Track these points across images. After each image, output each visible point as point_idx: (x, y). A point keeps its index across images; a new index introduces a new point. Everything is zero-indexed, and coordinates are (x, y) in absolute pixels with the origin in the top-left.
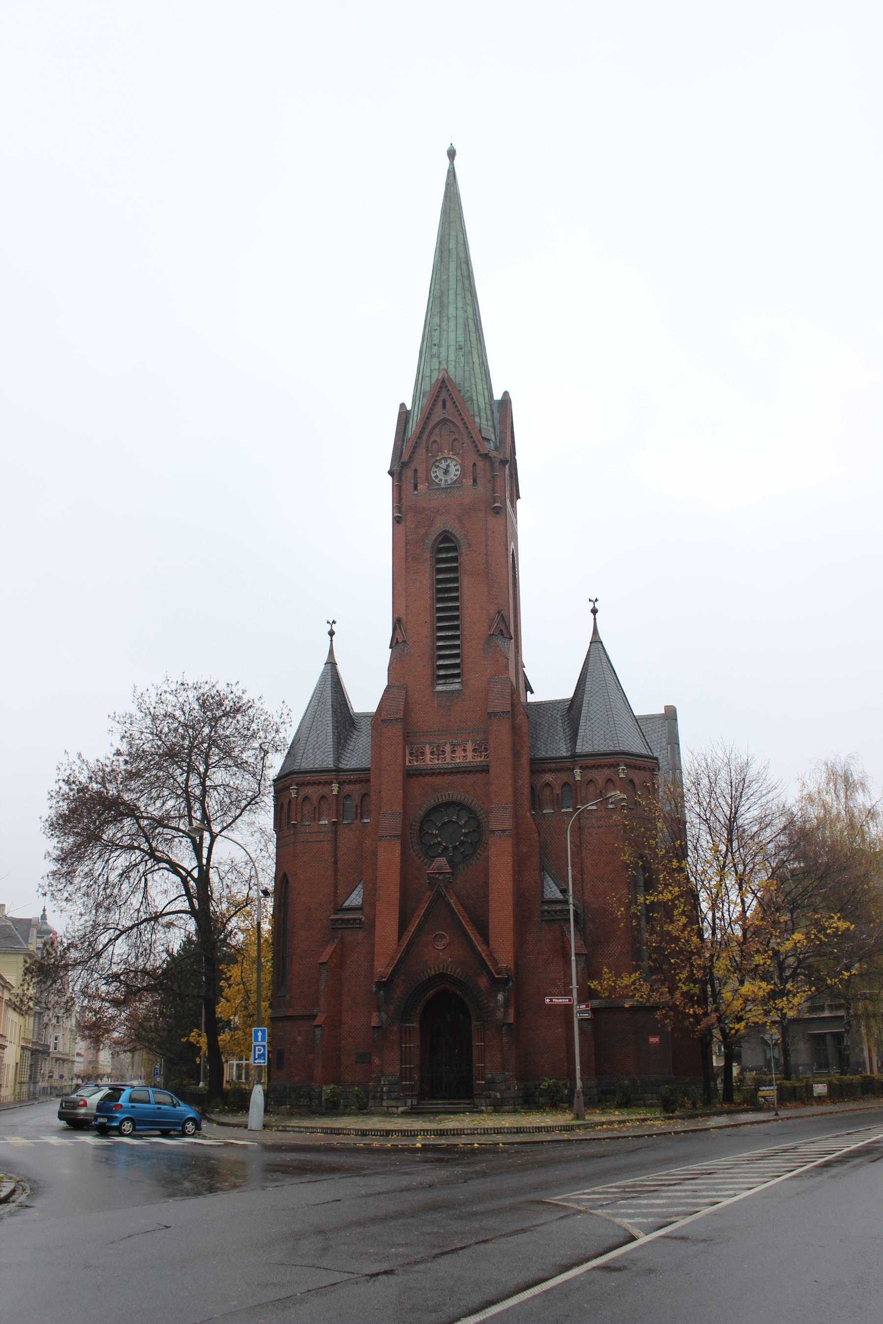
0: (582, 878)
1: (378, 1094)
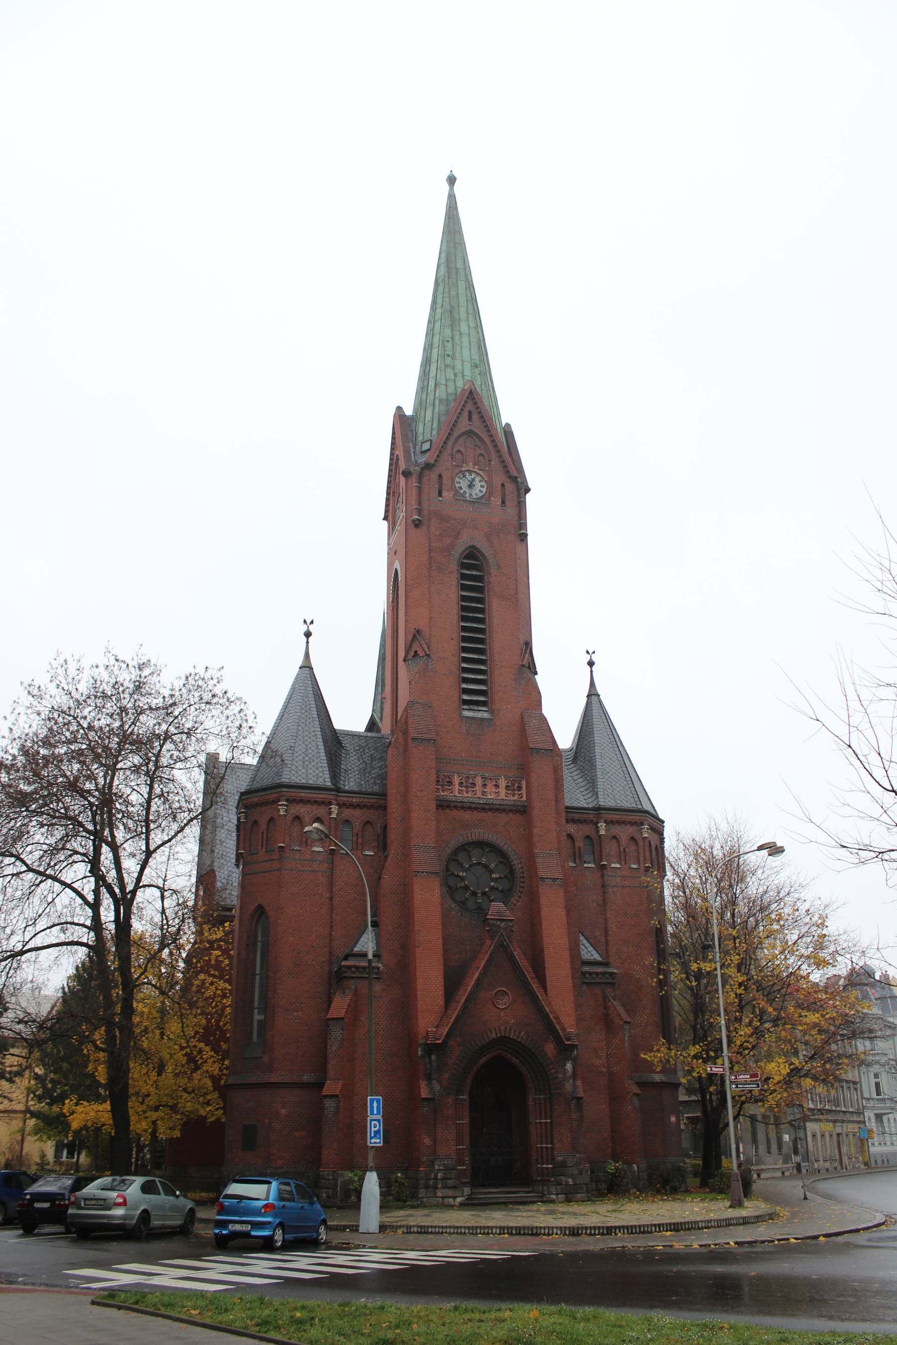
0: (606, 940)
1: (431, 1182)
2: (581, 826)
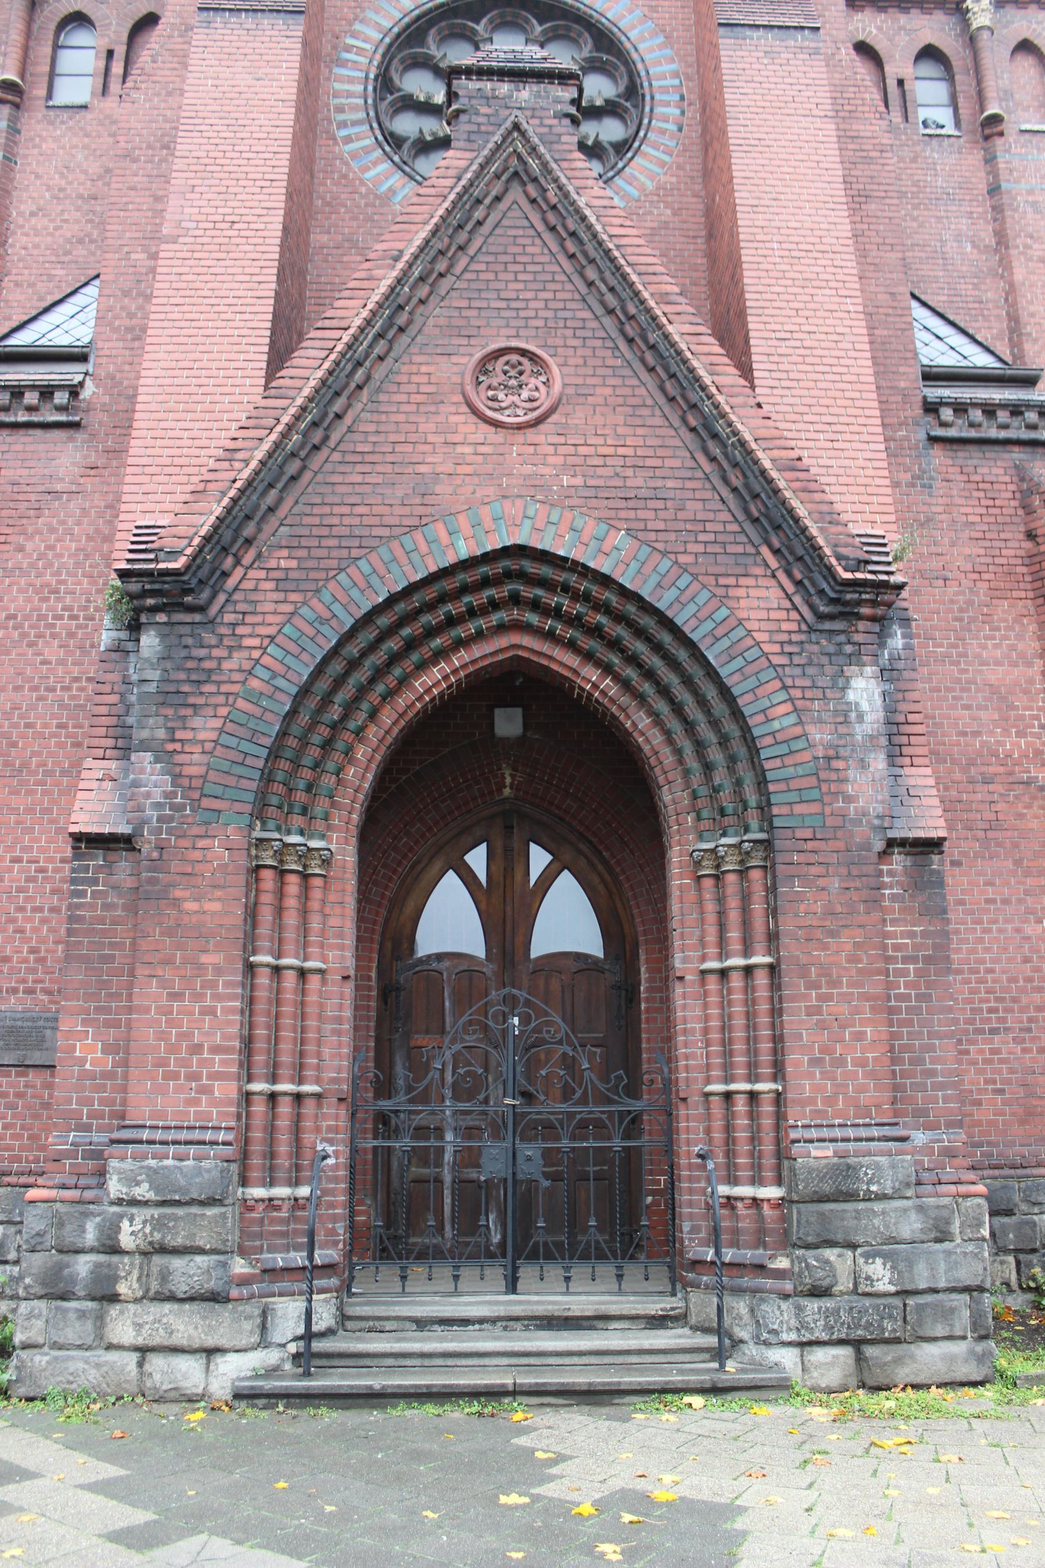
1: (83, 1266)
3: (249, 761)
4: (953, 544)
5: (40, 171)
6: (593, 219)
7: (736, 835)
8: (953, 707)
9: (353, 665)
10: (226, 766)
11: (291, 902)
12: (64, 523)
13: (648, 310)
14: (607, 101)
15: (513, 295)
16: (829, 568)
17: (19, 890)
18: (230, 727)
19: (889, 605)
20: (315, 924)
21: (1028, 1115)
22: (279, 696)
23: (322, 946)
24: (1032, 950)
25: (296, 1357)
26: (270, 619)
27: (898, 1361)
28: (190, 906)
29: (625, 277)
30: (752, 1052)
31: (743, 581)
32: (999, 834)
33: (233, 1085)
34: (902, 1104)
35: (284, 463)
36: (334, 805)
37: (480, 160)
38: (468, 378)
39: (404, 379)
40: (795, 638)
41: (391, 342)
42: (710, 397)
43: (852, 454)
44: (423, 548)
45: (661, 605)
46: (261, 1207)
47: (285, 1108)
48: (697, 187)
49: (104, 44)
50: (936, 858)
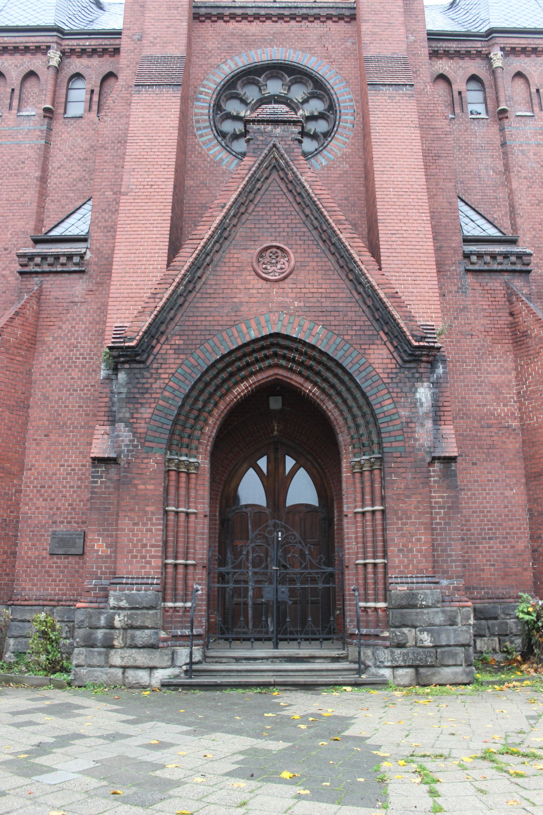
1: (100, 634)
2: (461, 63)
3: (164, 426)
4: (476, 319)
5: (61, 147)
6: (308, 187)
7: (369, 455)
8: (475, 394)
9: (207, 384)
10: (155, 428)
11: (183, 485)
12: (78, 316)
13: (332, 228)
14: (320, 113)
15: (273, 222)
16: (409, 341)
17: (64, 479)
18: (156, 412)
19: (435, 356)
20: (192, 494)
21: (506, 575)
22: (177, 399)
23: (195, 503)
24: (508, 502)
25: (186, 672)
26: (172, 366)
27: (433, 674)
28: (141, 487)
29: (322, 213)
30: (374, 546)
31: (372, 347)
32: (495, 451)
33: (159, 561)
34: (436, 569)
35: (177, 299)
36: (200, 443)
37: (259, 162)
38: (254, 260)
39: (227, 260)
40: (394, 371)
41: (221, 244)
42: (358, 266)
43: (422, 286)
44: (236, 334)
45: (336, 358)
46: (171, 610)
47: (181, 570)
48: (361, 154)
49: (89, 87)
50: (453, 464)
